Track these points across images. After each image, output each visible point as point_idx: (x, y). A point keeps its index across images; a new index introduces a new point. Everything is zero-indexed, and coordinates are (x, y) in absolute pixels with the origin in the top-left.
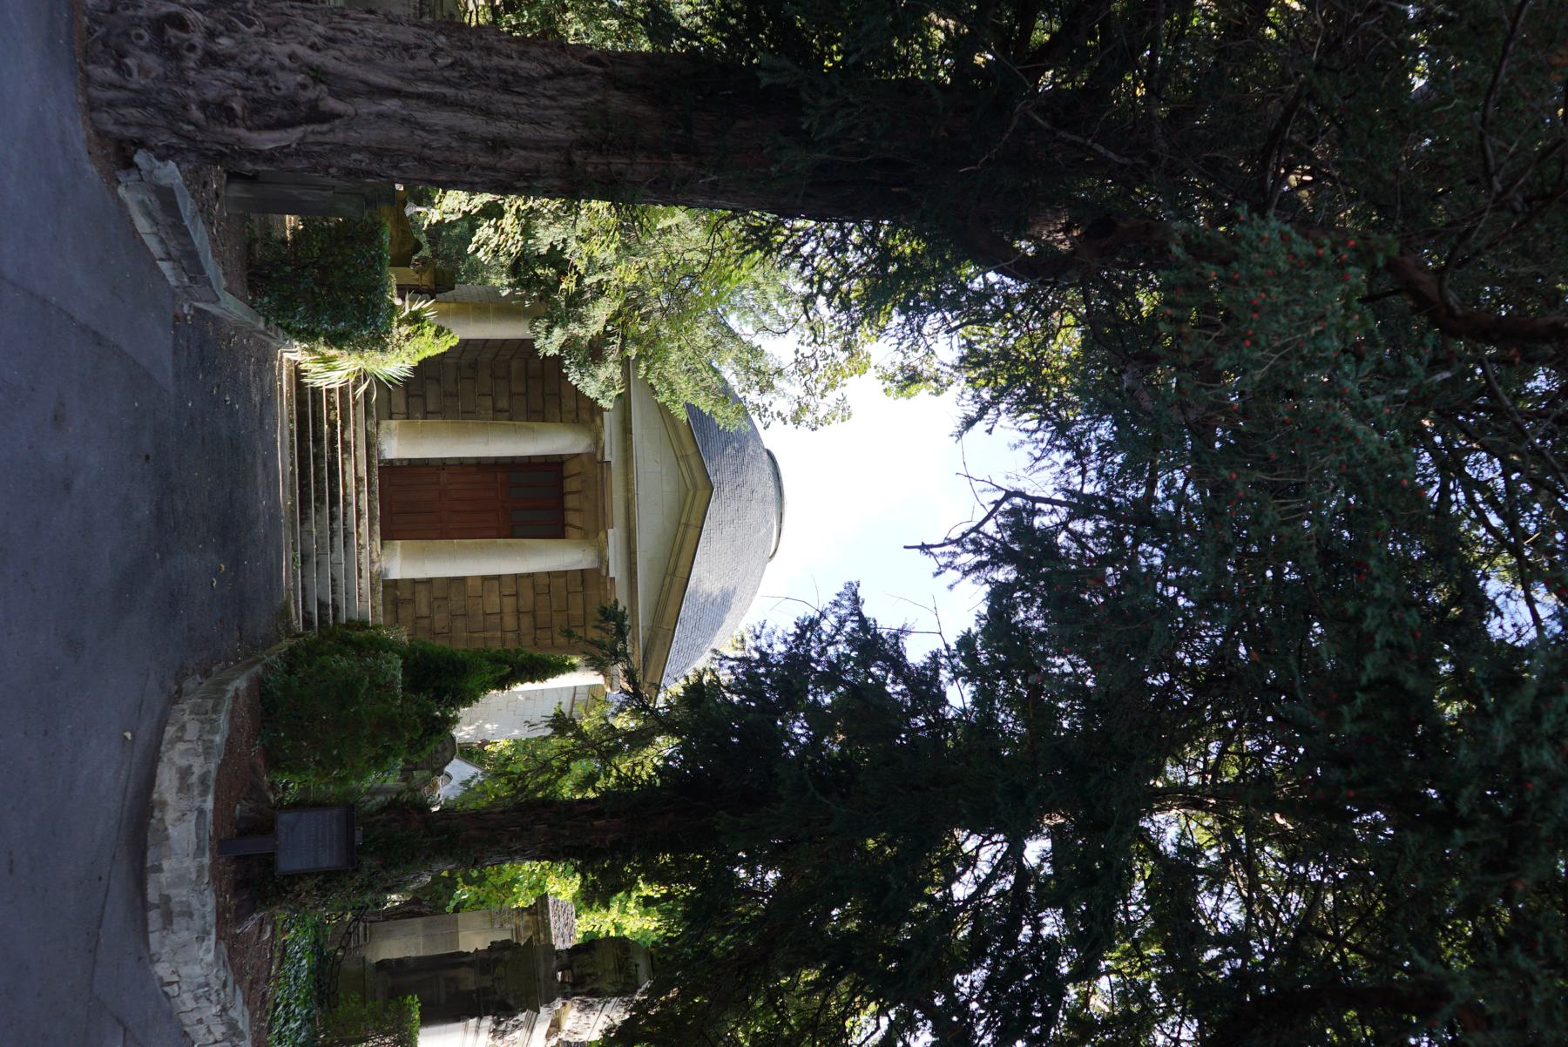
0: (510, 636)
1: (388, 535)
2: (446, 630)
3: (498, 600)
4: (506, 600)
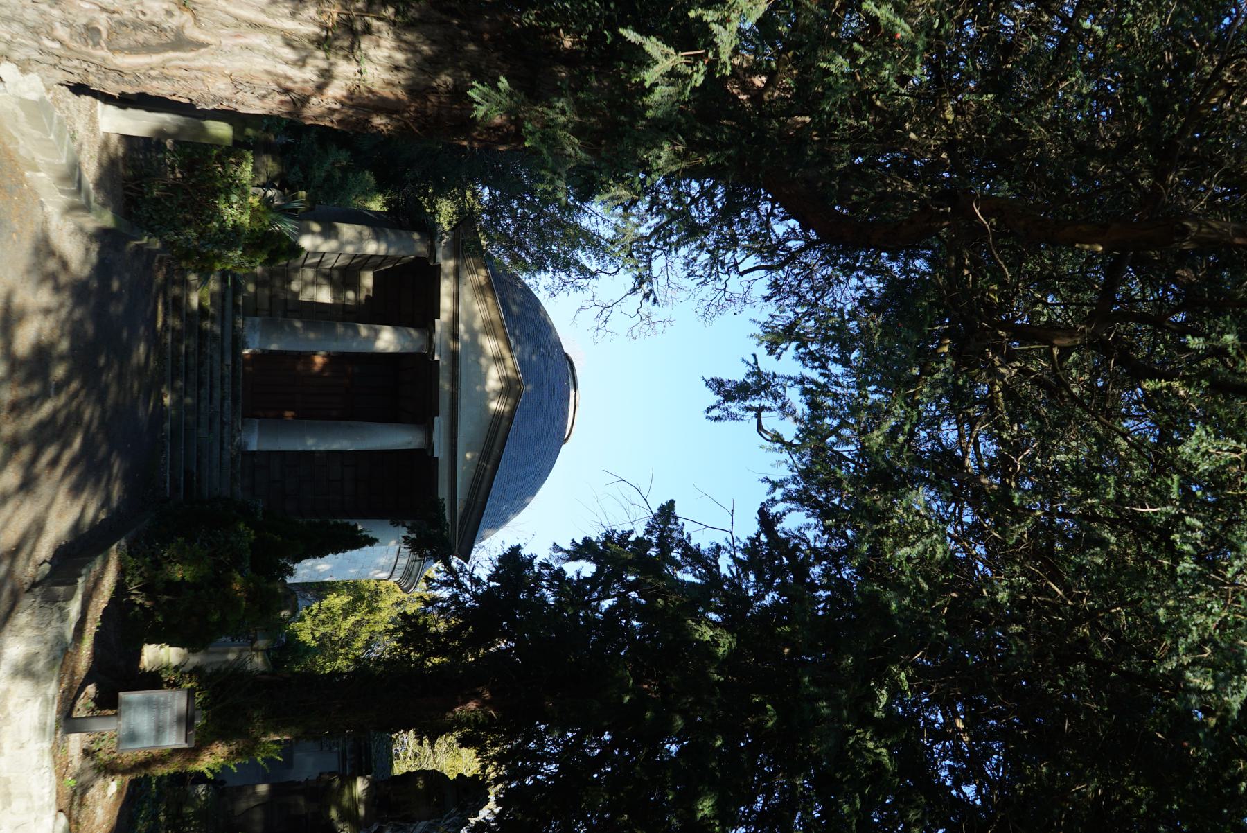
1: (249, 414)
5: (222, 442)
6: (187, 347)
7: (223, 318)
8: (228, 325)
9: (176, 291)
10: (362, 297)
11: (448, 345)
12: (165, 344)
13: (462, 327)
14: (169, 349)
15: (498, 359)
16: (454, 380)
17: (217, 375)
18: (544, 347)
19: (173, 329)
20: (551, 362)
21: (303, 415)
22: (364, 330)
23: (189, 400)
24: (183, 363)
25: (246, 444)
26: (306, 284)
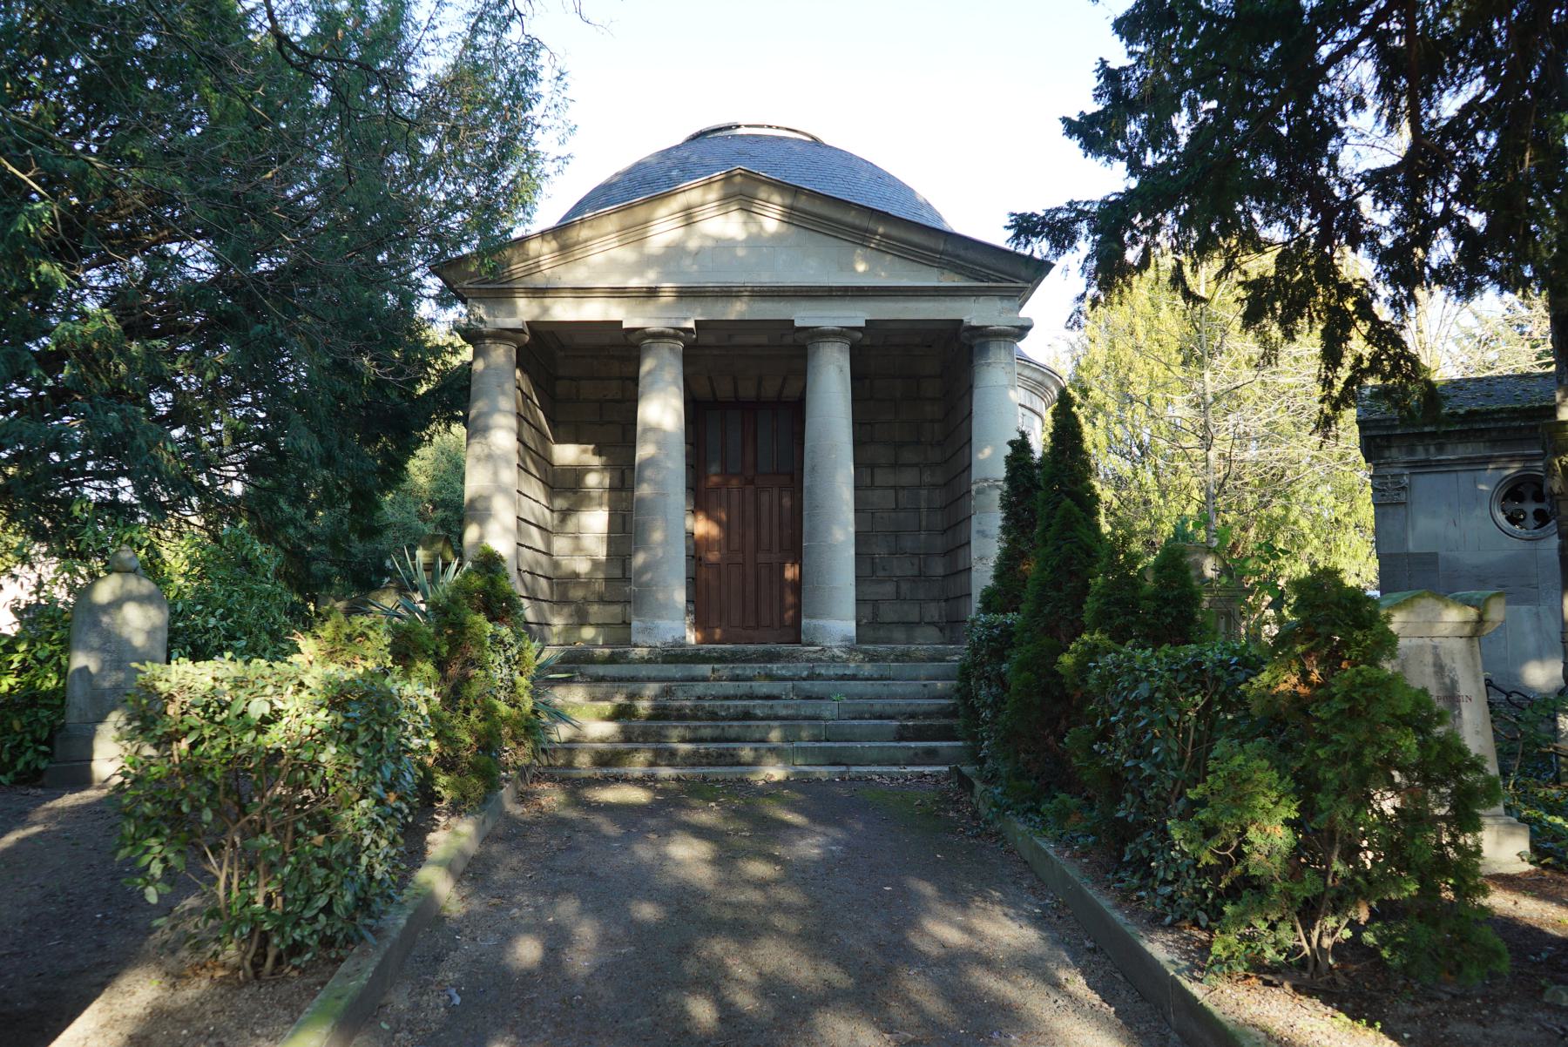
0: (927, 478)
1: (795, 634)
2: (916, 561)
3: (878, 492)
4: (879, 481)
5: (843, 678)
6: (683, 740)
7: (633, 679)
8: (644, 671)
9: (583, 761)
10: (596, 461)
11: (667, 305)
12: (678, 779)
13: (634, 282)
14: (687, 772)
15: (688, 216)
16: (727, 293)
17: (730, 687)
18: (670, 170)
19: (652, 764)
20: (694, 159)
21: (794, 546)
22: (644, 451)
23: (775, 735)
24: (713, 746)
25: (846, 639)
26: (578, 549)
